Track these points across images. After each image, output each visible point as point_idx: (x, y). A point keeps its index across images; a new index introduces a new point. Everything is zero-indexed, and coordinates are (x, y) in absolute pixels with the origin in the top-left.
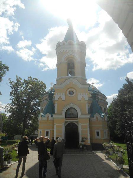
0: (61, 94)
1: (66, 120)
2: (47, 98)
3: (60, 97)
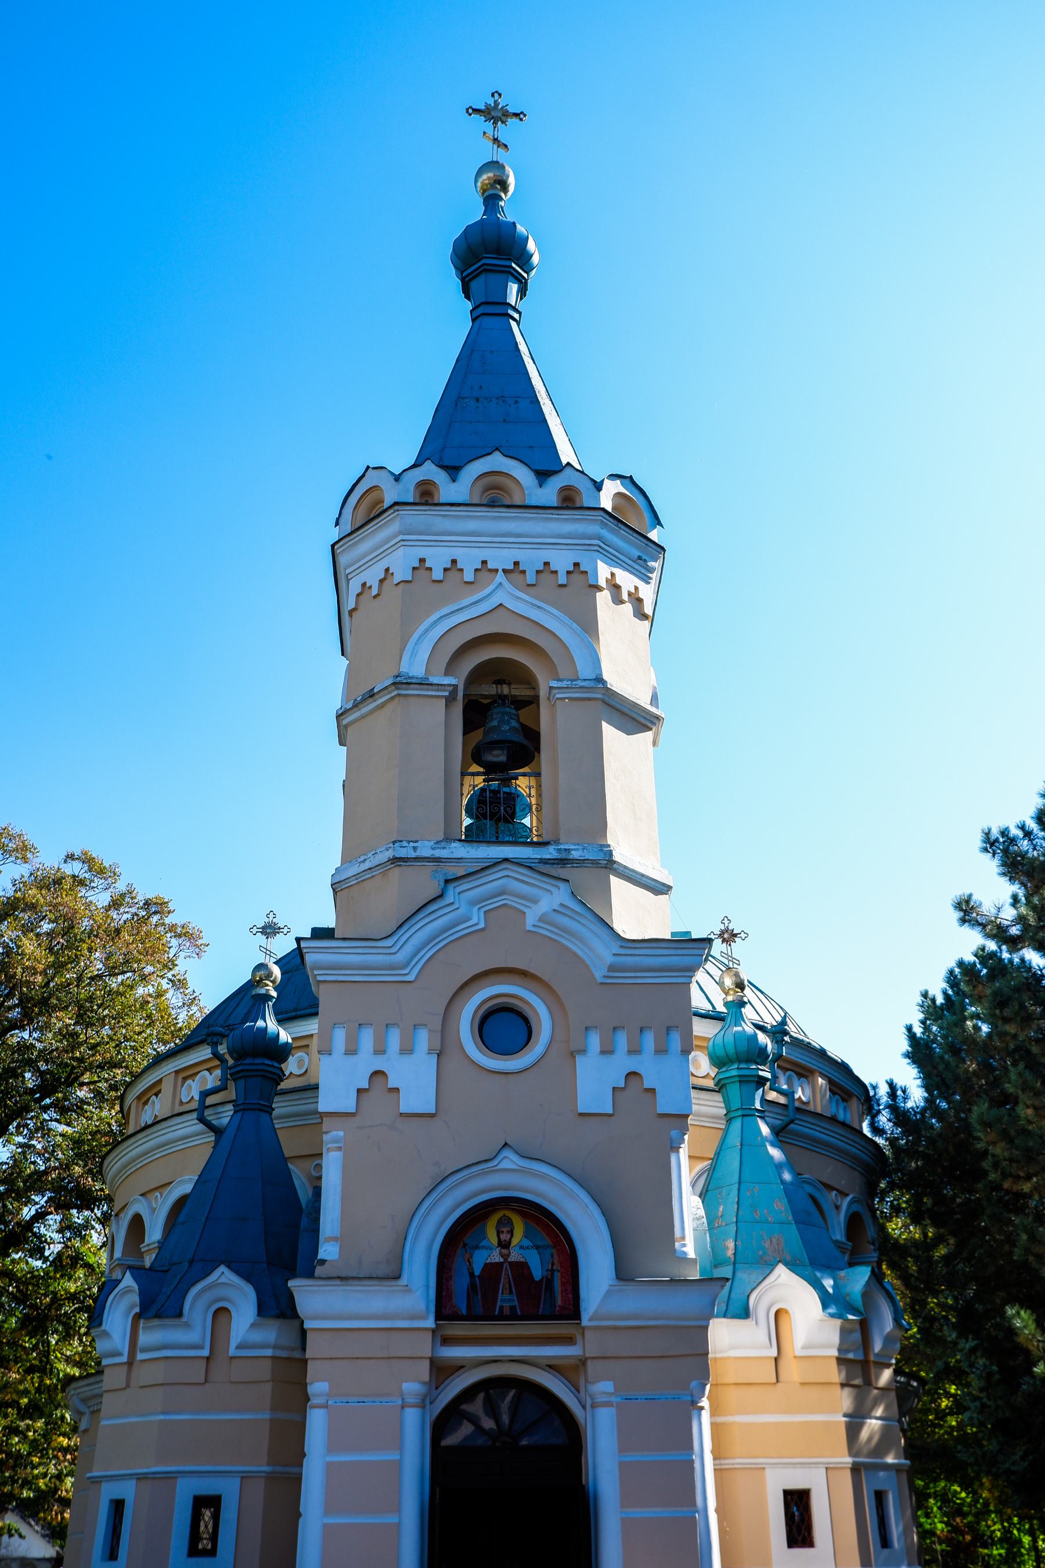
0: (394, 1040)
1: (446, 1341)
2: (205, 1094)
3: (632, 1075)
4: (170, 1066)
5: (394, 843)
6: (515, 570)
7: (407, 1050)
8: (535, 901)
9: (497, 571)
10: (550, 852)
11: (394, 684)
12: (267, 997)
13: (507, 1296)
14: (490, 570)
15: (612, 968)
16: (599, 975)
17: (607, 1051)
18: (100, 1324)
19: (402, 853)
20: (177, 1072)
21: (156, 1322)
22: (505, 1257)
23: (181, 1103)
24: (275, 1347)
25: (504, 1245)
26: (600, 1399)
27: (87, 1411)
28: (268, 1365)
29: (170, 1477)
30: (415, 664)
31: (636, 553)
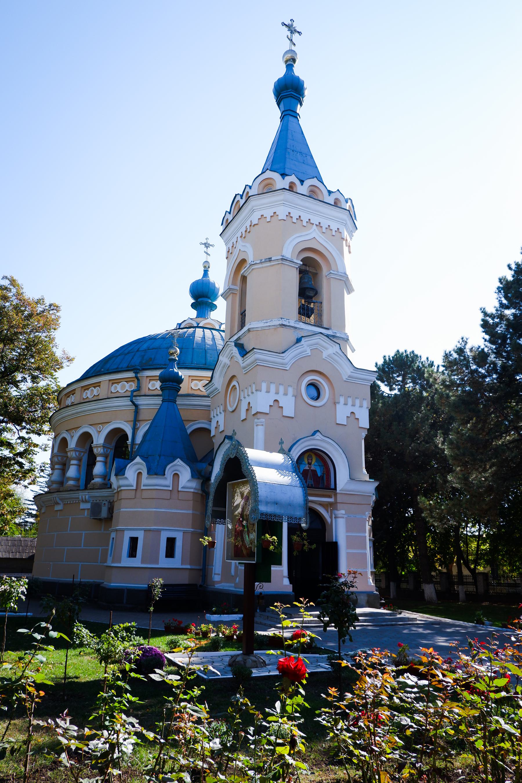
4: (107, 377)
5: (282, 318)
6: (319, 225)
7: (286, 394)
8: (327, 349)
9: (313, 224)
10: (329, 332)
11: (282, 259)
12: (175, 360)
13: (310, 481)
14: (311, 223)
15: (349, 377)
16: (345, 378)
17: (346, 404)
18: (124, 474)
19: (285, 323)
20: (110, 380)
21: (155, 476)
22: (310, 468)
23: (111, 392)
24: (195, 489)
25: (310, 464)
26: (340, 516)
27: (62, 503)
28: (191, 494)
29: (159, 531)
30: (288, 252)
31: (351, 229)
